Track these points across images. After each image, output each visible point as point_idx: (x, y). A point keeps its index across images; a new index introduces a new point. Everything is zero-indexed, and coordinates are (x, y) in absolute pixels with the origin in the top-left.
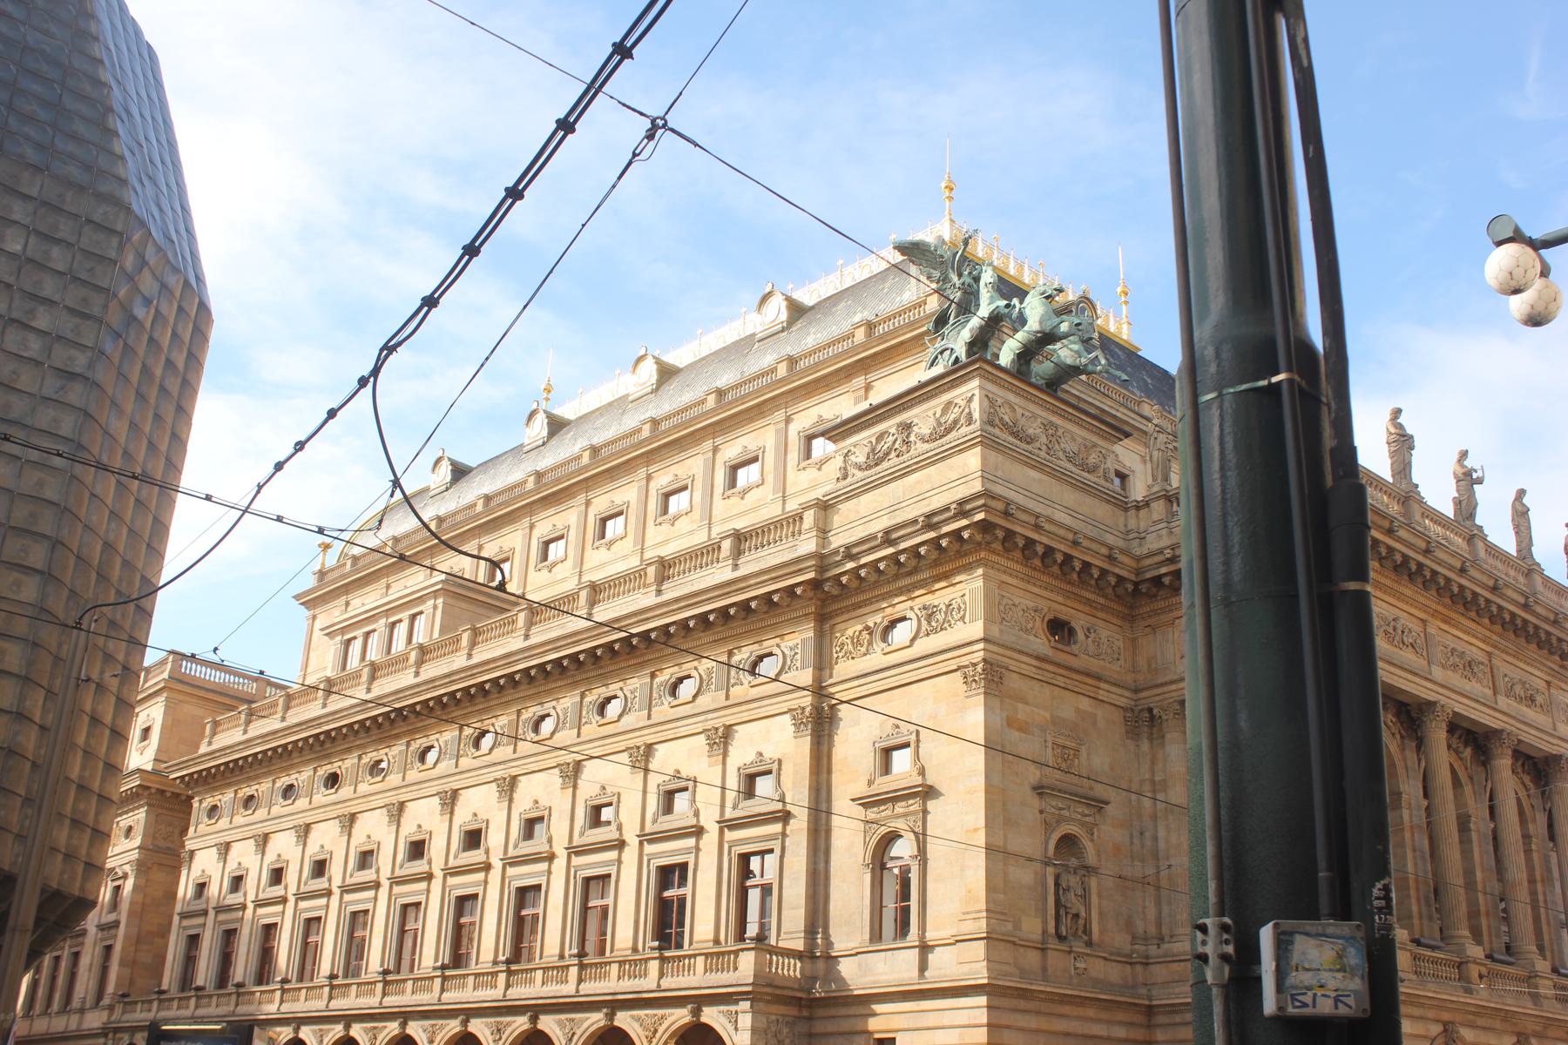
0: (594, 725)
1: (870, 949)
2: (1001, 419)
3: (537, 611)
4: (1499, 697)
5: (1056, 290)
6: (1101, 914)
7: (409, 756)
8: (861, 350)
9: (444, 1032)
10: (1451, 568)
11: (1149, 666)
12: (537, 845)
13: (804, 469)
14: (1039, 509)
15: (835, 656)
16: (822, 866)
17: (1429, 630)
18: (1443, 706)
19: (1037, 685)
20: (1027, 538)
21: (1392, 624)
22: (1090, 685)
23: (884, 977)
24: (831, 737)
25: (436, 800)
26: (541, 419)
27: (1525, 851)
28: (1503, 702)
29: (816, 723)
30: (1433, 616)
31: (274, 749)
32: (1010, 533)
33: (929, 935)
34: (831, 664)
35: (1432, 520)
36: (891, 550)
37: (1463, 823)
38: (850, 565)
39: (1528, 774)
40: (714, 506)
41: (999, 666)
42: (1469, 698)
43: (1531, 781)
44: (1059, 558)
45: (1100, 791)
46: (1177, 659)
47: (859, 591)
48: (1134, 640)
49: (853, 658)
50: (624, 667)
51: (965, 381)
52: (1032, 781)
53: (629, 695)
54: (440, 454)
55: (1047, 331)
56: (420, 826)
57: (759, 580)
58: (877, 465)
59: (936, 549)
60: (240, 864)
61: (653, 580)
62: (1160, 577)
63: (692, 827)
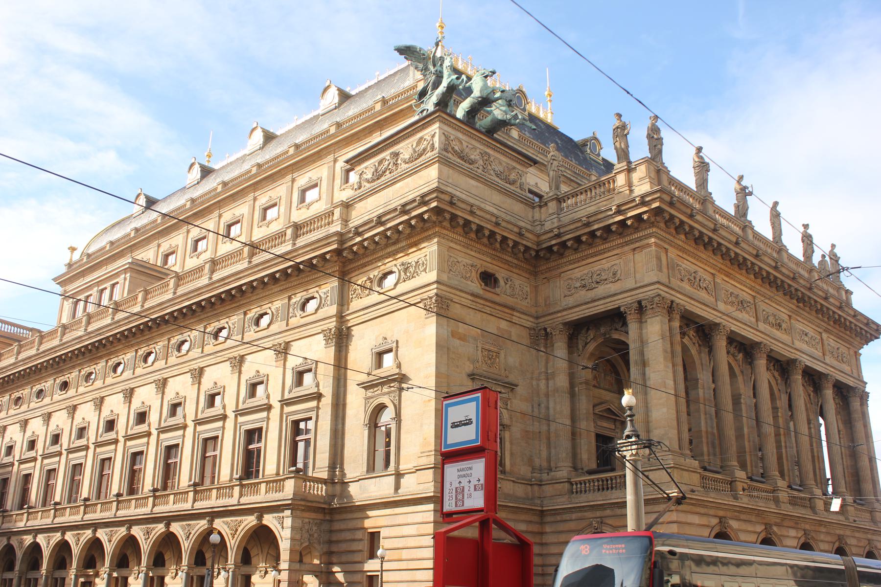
0: (211, 345)
1: (367, 477)
2: (453, 148)
3: (179, 278)
4: (759, 323)
5: (491, 72)
6: (512, 454)
7: (107, 369)
8: (378, 115)
9: (117, 535)
10: (730, 242)
11: (546, 301)
12: (178, 420)
13: (344, 189)
14: (472, 201)
15: (351, 297)
16: (340, 426)
17: (717, 280)
18: (724, 326)
19: (472, 312)
20: (465, 219)
21: (693, 274)
22: (507, 313)
23: (373, 494)
24: (347, 347)
25: (121, 395)
26: (197, 168)
27: (773, 417)
28: (762, 326)
29: (338, 338)
30: (719, 271)
31: (30, 368)
32: (454, 217)
33: (401, 467)
34: (348, 301)
35: (720, 215)
36: (382, 229)
37: (736, 400)
38: (358, 239)
39: (777, 371)
40: (292, 214)
41: (446, 299)
42: (697, 301)
43: (779, 375)
44: (487, 233)
45: (512, 378)
46: (562, 297)
47: (365, 255)
48: (536, 287)
49: (361, 298)
50: (229, 309)
51: (431, 125)
52: (468, 371)
53: (231, 326)
54: (139, 191)
55: (484, 97)
56: (112, 411)
57: (304, 251)
58: (378, 179)
59: (409, 227)
60: (11, 438)
61: (247, 256)
62: (552, 246)
63: (265, 405)
